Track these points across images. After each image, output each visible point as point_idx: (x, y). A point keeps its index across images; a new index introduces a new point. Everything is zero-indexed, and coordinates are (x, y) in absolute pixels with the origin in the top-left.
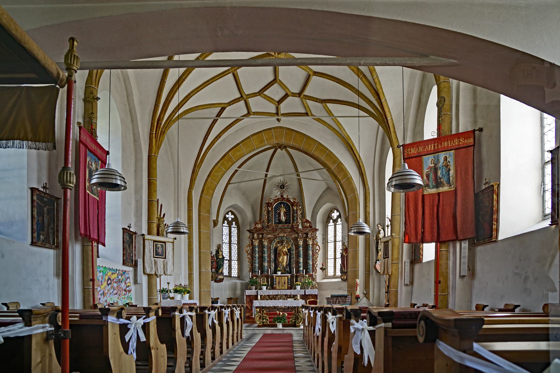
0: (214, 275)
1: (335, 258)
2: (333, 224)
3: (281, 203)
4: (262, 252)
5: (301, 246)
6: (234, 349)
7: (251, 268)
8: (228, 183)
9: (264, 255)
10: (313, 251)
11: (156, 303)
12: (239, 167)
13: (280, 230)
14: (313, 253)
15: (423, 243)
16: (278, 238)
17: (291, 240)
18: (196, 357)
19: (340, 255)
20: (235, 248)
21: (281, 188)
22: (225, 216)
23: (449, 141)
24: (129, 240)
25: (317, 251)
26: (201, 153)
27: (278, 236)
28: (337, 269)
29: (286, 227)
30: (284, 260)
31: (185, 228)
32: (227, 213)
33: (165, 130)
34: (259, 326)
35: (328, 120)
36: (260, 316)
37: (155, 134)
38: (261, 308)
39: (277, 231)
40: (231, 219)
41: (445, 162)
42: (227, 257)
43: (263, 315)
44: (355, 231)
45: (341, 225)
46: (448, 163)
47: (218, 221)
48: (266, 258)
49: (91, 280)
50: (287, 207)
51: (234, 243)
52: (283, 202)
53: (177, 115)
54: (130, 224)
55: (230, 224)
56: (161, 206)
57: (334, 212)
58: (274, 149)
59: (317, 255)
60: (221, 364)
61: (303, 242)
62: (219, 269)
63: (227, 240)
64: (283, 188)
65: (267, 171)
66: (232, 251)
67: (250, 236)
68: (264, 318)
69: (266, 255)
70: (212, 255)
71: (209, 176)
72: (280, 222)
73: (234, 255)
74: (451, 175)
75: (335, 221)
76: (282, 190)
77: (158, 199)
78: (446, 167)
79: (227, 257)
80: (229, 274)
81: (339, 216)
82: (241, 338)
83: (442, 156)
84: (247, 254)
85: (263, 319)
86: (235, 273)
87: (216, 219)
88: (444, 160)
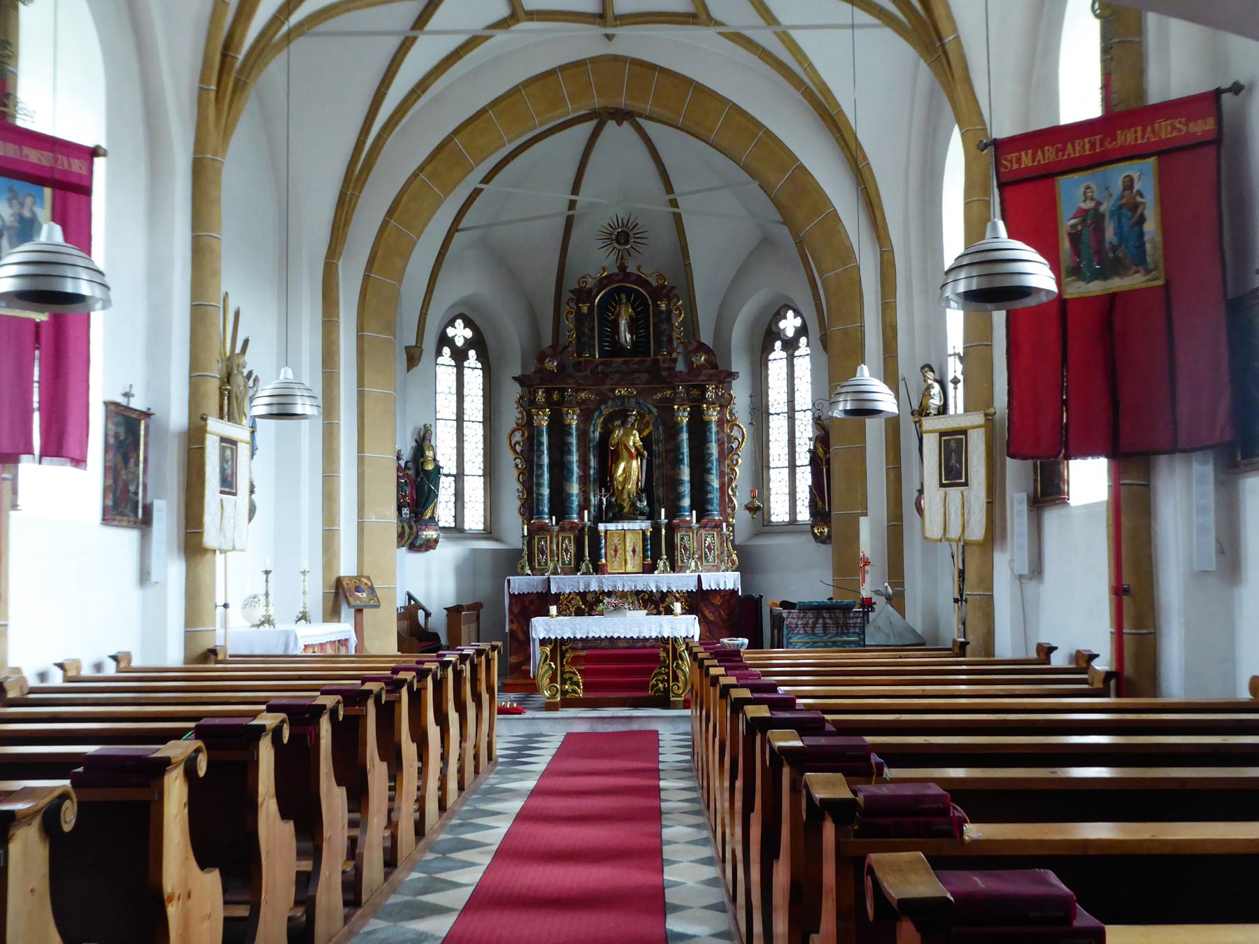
0: (407, 529)
1: (792, 467)
2: (784, 354)
3: (619, 290)
5: (685, 429)
6: (465, 808)
7: (526, 500)
8: (454, 229)
10: (723, 443)
11: (211, 646)
12: (487, 179)
13: (618, 375)
14: (721, 452)
15: (1067, 457)
16: (610, 403)
17: (651, 407)
18: (329, 878)
19: (808, 455)
20: (475, 435)
21: (619, 243)
24: (125, 439)
25: (735, 446)
27: (611, 395)
28: (799, 503)
29: (636, 366)
30: (630, 471)
31: (308, 401)
32: (451, 323)
34: (551, 707)
35: (766, 38)
36: (555, 672)
37: (217, 92)
38: (558, 647)
39: (608, 381)
41: (1127, 193)
43: (562, 666)
45: (808, 358)
46: (1139, 199)
47: (421, 353)
48: (575, 469)
50: (639, 304)
53: (285, 29)
54: (131, 386)
55: (459, 356)
56: (237, 314)
57: (785, 318)
59: (736, 457)
60: (419, 878)
61: (689, 414)
62: (425, 507)
64: (627, 242)
65: (576, 189)
68: (567, 676)
70: (402, 463)
71: (391, 212)
72: (617, 349)
74: (1147, 238)
75: (790, 346)
76: (621, 247)
77: (227, 294)
78: (1130, 210)
80: (455, 521)
81: (802, 331)
82: (490, 758)
83: (1117, 174)
84: (511, 455)
85: (564, 682)
87: (414, 344)
88: (1124, 190)
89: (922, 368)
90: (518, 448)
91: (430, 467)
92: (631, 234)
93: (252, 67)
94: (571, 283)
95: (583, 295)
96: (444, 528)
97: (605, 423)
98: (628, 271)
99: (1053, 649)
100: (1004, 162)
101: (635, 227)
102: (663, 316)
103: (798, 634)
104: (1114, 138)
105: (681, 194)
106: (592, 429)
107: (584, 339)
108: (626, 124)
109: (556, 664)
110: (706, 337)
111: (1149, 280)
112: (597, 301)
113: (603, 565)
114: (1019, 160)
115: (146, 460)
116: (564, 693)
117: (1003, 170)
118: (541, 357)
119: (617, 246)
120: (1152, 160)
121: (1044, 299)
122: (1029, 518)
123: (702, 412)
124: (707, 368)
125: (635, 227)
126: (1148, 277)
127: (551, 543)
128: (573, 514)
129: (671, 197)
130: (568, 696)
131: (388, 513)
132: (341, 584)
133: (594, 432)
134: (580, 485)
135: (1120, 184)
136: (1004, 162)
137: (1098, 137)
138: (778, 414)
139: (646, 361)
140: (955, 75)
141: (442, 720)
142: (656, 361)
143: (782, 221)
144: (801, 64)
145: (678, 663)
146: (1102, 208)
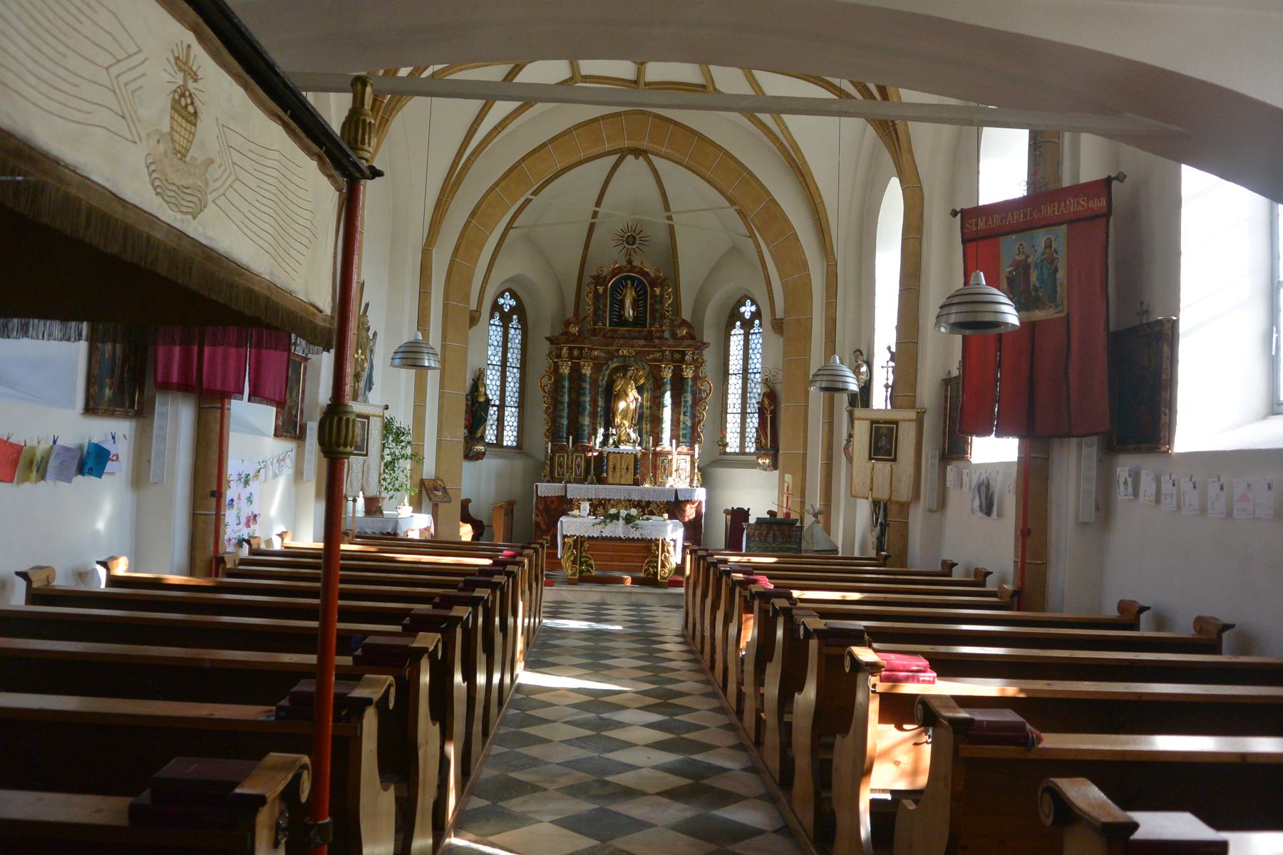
2: (742, 332)
4: (577, 391)
8: (509, 227)
9: (582, 398)
12: (535, 193)
14: (694, 399)
20: (513, 376)
21: (628, 243)
22: (496, 303)
23: (1056, 204)
25: (704, 395)
26: (458, 163)
29: (636, 334)
32: (502, 295)
33: (390, 117)
36: (576, 557)
40: (508, 307)
42: (495, 399)
43: (581, 552)
44: (824, 385)
46: (1055, 255)
47: (480, 315)
48: (588, 407)
49: (213, 494)
51: (513, 365)
52: (629, 277)
55: (506, 320)
58: (619, 155)
61: (673, 371)
63: (497, 359)
64: (634, 243)
66: (507, 384)
67: (550, 353)
69: (588, 399)
71: (473, 214)
72: (621, 321)
73: (512, 395)
75: (747, 325)
76: (630, 247)
79: (495, 397)
80: (497, 439)
83: (1041, 237)
85: (581, 564)
86: (512, 438)
87: (475, 309)
88: (1046, 248)
89: (855, 352)
90: (546, 389)
91: (482, 399)
92: (637, 237)
93: (393, 109)
94: (591, 271)
95: (599, 280)
96: (488, 444)
97: (610, 376)
98: (634, 264)
99: (954, 565)
100: (967, 225)
101: (640, 232)
102: (658, 299)
103: (754, 541)
104: (1040, 211)
105: (674, 213)
106: (601, 378)
107: (600, 312)
108: (641, 158)
109: (576, 551)
110: (686, 314)
111: (1057, 313)
112: (610, 285)
113: (604, 477)
114: (977, 225)
115: (303, 391)
116: (581, 572)
117: (966, 230)
118: (567, 324)
119: (627, 246)
120: (1064, 227)
121: (1010, 329)
122: (939, 468)
123: (682, 370)
124: (687, 339)
125: (640, 232)
126: (1057, 310)
127: (568, 459)
128: (584, 439)
129: (668, 214)
130: (584, 574)
131: (459, 435)
132: (424, 483)
133: (602, 380)
134: (590, 418)
135: (1043, 245)
136: (967, 225)
137: (1029, 209)
138: (736, 374)
139: (643, 331)
140: (902, 147)
141: (703, 637)
142: (650, 332)
143: (749, 235)
144: (779, 126)
145: (665, 557)
146: (1030, 260)
